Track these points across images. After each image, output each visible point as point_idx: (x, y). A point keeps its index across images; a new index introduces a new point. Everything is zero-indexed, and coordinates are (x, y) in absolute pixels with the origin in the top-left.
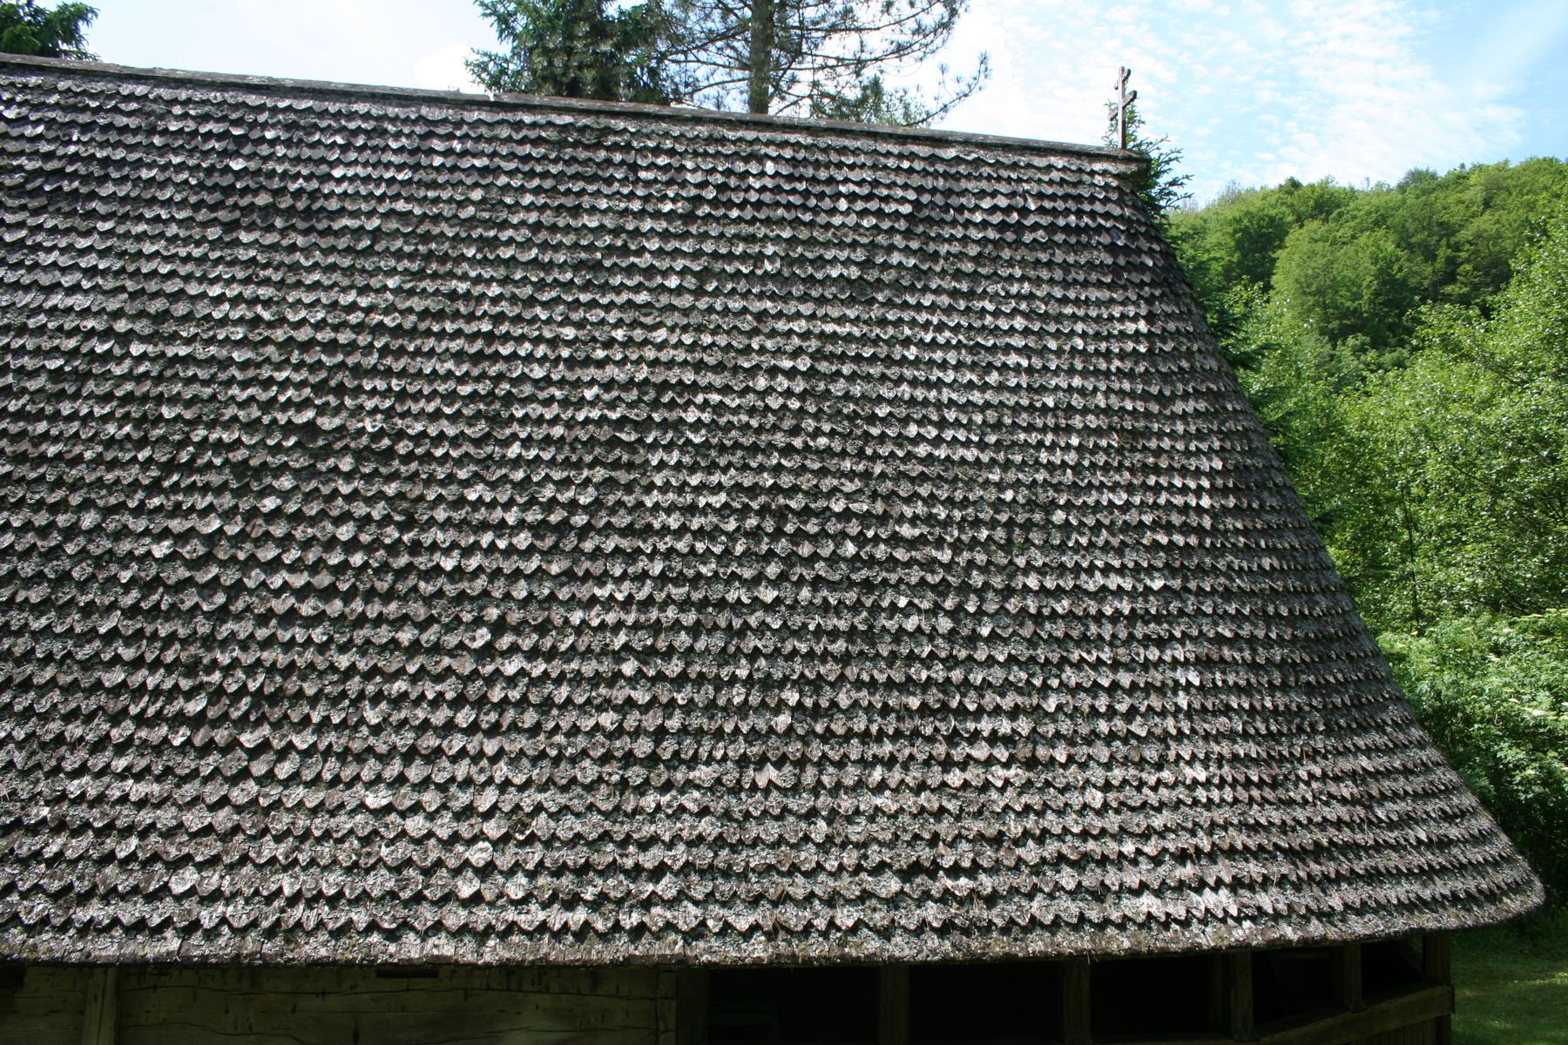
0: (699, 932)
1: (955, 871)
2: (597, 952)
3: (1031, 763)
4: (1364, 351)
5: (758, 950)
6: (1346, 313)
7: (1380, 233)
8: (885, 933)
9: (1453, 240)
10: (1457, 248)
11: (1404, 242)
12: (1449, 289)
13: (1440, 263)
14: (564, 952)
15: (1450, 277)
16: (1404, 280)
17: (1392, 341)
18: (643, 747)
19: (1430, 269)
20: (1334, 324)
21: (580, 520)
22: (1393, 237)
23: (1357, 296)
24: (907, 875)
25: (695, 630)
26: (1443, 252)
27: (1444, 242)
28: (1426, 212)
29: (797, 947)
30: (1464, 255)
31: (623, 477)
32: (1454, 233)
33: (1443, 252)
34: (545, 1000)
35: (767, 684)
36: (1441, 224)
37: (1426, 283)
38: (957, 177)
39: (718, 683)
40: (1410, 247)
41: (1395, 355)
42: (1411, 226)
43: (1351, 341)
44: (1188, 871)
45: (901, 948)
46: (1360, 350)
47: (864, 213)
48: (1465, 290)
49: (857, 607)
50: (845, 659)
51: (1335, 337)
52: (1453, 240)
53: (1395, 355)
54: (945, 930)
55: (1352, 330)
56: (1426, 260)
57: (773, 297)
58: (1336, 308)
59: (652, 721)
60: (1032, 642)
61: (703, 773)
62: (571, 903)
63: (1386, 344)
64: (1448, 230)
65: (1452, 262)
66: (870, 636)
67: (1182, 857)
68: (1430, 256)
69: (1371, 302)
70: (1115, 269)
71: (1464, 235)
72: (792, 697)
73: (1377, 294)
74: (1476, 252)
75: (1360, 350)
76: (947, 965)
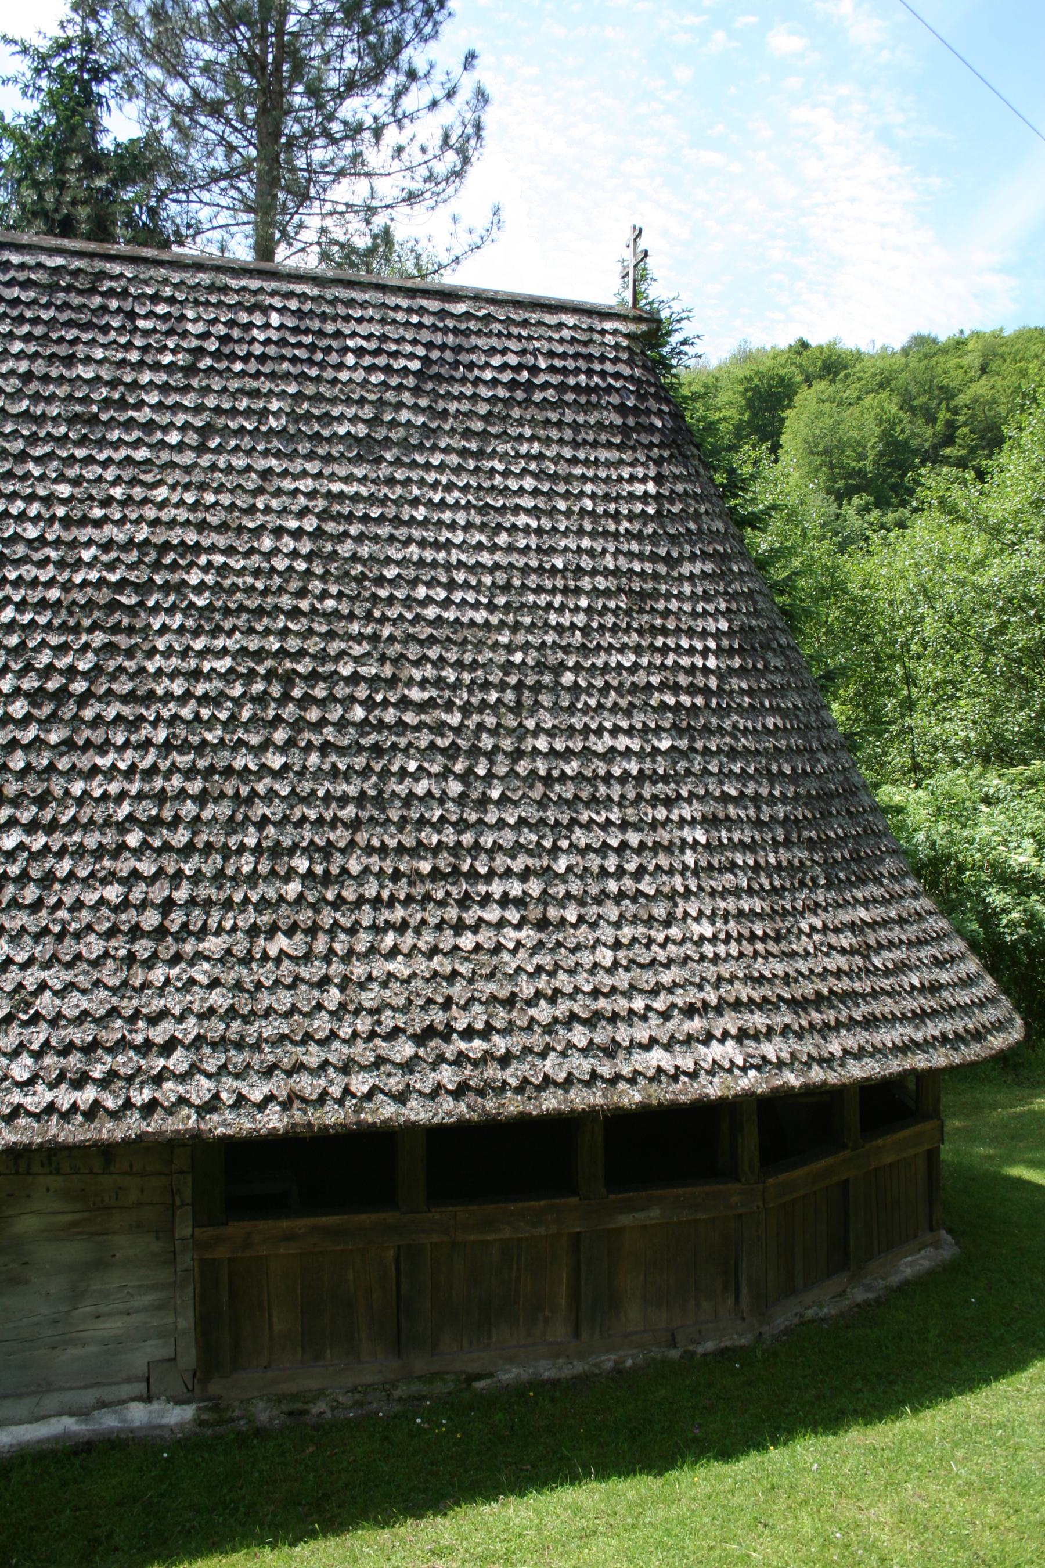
0: (212, 1105)
1: (469, 1034)
2: (109, 1131)
3: (543, 924)
4: (869, 511)
5: (274, 1120)
6: (851, 474)
7: (884, 395)
8: (401, 1098)
9: (952, 404)
10: (956, 412)
11: (907, 404)
12: (948, 451)
13: (940, 426)
14: (75, 1132)
15: (949, 440)
16: (906, 442)
17: (895, 501)
18: (150, 920)
19: (930, 432)
20: (840, 484)
21: (79, 686)
22: (896, 399)
23: (861, 457)
24: (421, 1039)
25: (202, 799)
26: (943, 415)
27: (943, 405)
28: (927, 376)
29: (314, 1116)
30: (962, 419)
31: (123, 641)
32: (953, 397)
33: (943, 415)
34: (56, 1182)
35: (276, 851)
36: (941, 388)
37: (927, 445)
38: (467, 333)
39: (227, 854)
40: (913, 410)
41: (897, 514)
42: (913, 389)
43: (855, 500)
44: (695, 1025)
45: (417, 1112)
46: (866, 509)
47: (372, 368)
48: (963, 452)
49: (366, 772)
50: (355, 825)
51: (841, 496)
52: (952, 404)
53: (897, 514)
54: (460, 1092)
55: (856, 490)
56: (927, 423)
57: (278, 455)
58: (842, 468)
59: (158, 893)
60: (542, 804)
61: (213, 945)
62: (79, 1082)
63: (889, 504)
64: (947, 394)
65: (951, 425)
66: (380, 801)
67: (690, 1011)
68: (931, 419)
69: (875, 463)
70: (625, 430)
71: (962, 399)
72: (302, 864)
73: (881, 455)
74: (972, 416)
75: (866, 509)
76: (461, 1129)
